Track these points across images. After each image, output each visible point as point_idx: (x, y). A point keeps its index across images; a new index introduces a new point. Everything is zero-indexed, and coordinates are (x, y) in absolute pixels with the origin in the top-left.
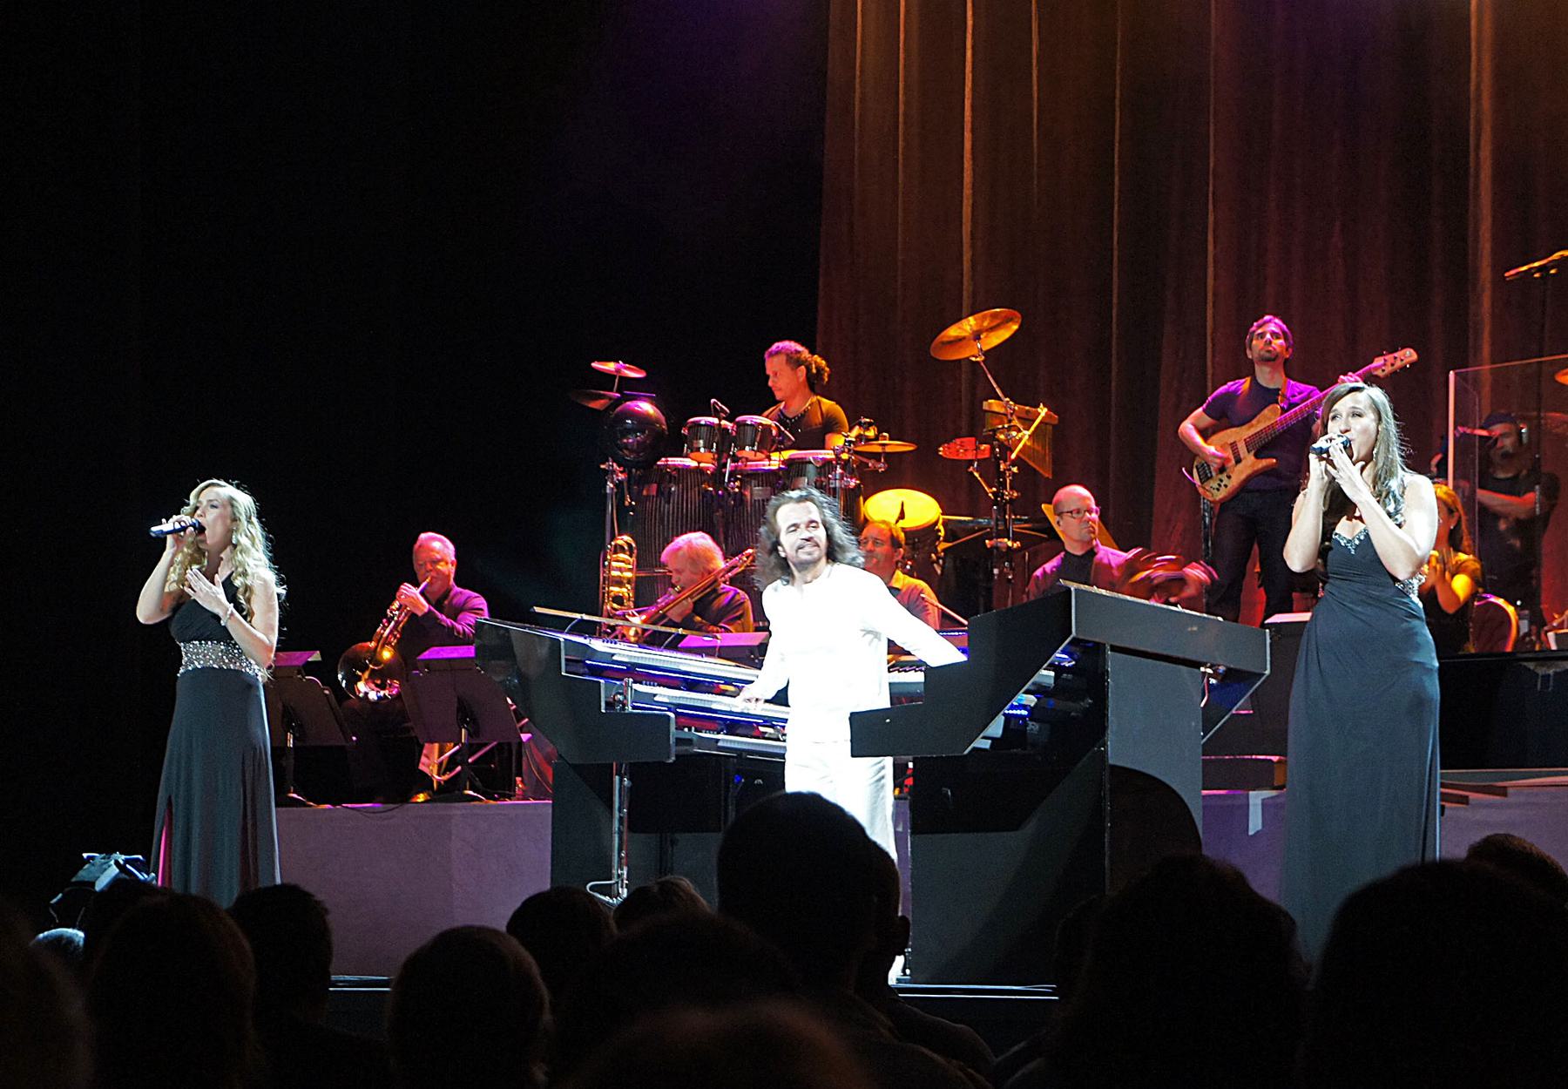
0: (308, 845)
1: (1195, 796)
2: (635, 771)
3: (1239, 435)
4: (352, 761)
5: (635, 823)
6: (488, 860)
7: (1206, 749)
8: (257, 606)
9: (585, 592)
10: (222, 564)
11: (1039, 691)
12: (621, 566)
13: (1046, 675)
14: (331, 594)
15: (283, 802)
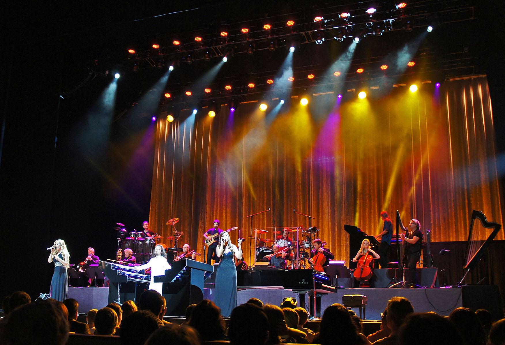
0: (70, 292)
1: (203, 289)
2: (121, 284)
3: (212, 237)
4: (77, 280)
5: (121, 292)
6: (99, 297)
7: (204, 282)
8: (65, 257)
9: (114, 257)
10: (60, 252)
11: (181, 273)
12: (120, 253)
13: (182, 271)
14: (77, 256)
15: (69, 286)
